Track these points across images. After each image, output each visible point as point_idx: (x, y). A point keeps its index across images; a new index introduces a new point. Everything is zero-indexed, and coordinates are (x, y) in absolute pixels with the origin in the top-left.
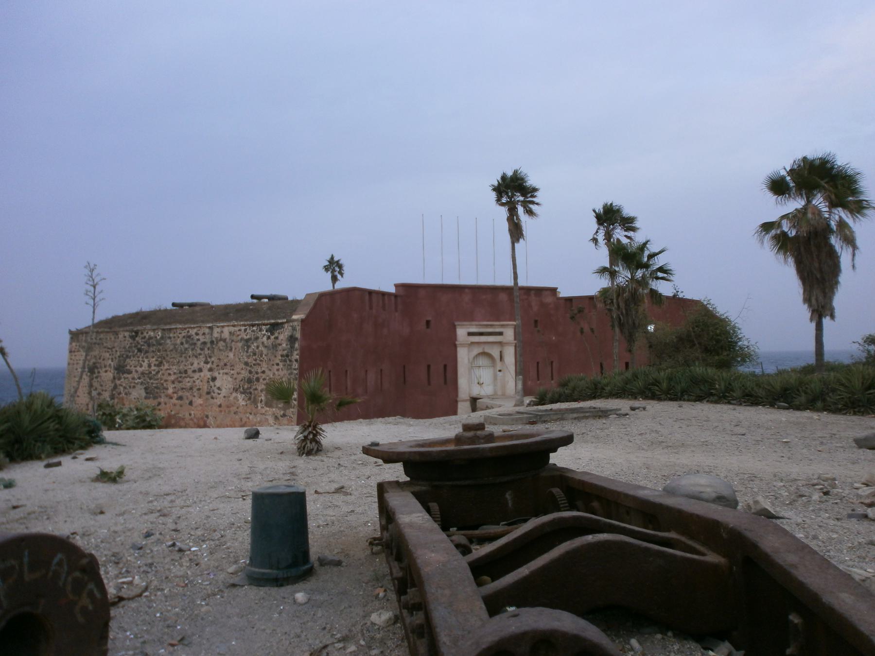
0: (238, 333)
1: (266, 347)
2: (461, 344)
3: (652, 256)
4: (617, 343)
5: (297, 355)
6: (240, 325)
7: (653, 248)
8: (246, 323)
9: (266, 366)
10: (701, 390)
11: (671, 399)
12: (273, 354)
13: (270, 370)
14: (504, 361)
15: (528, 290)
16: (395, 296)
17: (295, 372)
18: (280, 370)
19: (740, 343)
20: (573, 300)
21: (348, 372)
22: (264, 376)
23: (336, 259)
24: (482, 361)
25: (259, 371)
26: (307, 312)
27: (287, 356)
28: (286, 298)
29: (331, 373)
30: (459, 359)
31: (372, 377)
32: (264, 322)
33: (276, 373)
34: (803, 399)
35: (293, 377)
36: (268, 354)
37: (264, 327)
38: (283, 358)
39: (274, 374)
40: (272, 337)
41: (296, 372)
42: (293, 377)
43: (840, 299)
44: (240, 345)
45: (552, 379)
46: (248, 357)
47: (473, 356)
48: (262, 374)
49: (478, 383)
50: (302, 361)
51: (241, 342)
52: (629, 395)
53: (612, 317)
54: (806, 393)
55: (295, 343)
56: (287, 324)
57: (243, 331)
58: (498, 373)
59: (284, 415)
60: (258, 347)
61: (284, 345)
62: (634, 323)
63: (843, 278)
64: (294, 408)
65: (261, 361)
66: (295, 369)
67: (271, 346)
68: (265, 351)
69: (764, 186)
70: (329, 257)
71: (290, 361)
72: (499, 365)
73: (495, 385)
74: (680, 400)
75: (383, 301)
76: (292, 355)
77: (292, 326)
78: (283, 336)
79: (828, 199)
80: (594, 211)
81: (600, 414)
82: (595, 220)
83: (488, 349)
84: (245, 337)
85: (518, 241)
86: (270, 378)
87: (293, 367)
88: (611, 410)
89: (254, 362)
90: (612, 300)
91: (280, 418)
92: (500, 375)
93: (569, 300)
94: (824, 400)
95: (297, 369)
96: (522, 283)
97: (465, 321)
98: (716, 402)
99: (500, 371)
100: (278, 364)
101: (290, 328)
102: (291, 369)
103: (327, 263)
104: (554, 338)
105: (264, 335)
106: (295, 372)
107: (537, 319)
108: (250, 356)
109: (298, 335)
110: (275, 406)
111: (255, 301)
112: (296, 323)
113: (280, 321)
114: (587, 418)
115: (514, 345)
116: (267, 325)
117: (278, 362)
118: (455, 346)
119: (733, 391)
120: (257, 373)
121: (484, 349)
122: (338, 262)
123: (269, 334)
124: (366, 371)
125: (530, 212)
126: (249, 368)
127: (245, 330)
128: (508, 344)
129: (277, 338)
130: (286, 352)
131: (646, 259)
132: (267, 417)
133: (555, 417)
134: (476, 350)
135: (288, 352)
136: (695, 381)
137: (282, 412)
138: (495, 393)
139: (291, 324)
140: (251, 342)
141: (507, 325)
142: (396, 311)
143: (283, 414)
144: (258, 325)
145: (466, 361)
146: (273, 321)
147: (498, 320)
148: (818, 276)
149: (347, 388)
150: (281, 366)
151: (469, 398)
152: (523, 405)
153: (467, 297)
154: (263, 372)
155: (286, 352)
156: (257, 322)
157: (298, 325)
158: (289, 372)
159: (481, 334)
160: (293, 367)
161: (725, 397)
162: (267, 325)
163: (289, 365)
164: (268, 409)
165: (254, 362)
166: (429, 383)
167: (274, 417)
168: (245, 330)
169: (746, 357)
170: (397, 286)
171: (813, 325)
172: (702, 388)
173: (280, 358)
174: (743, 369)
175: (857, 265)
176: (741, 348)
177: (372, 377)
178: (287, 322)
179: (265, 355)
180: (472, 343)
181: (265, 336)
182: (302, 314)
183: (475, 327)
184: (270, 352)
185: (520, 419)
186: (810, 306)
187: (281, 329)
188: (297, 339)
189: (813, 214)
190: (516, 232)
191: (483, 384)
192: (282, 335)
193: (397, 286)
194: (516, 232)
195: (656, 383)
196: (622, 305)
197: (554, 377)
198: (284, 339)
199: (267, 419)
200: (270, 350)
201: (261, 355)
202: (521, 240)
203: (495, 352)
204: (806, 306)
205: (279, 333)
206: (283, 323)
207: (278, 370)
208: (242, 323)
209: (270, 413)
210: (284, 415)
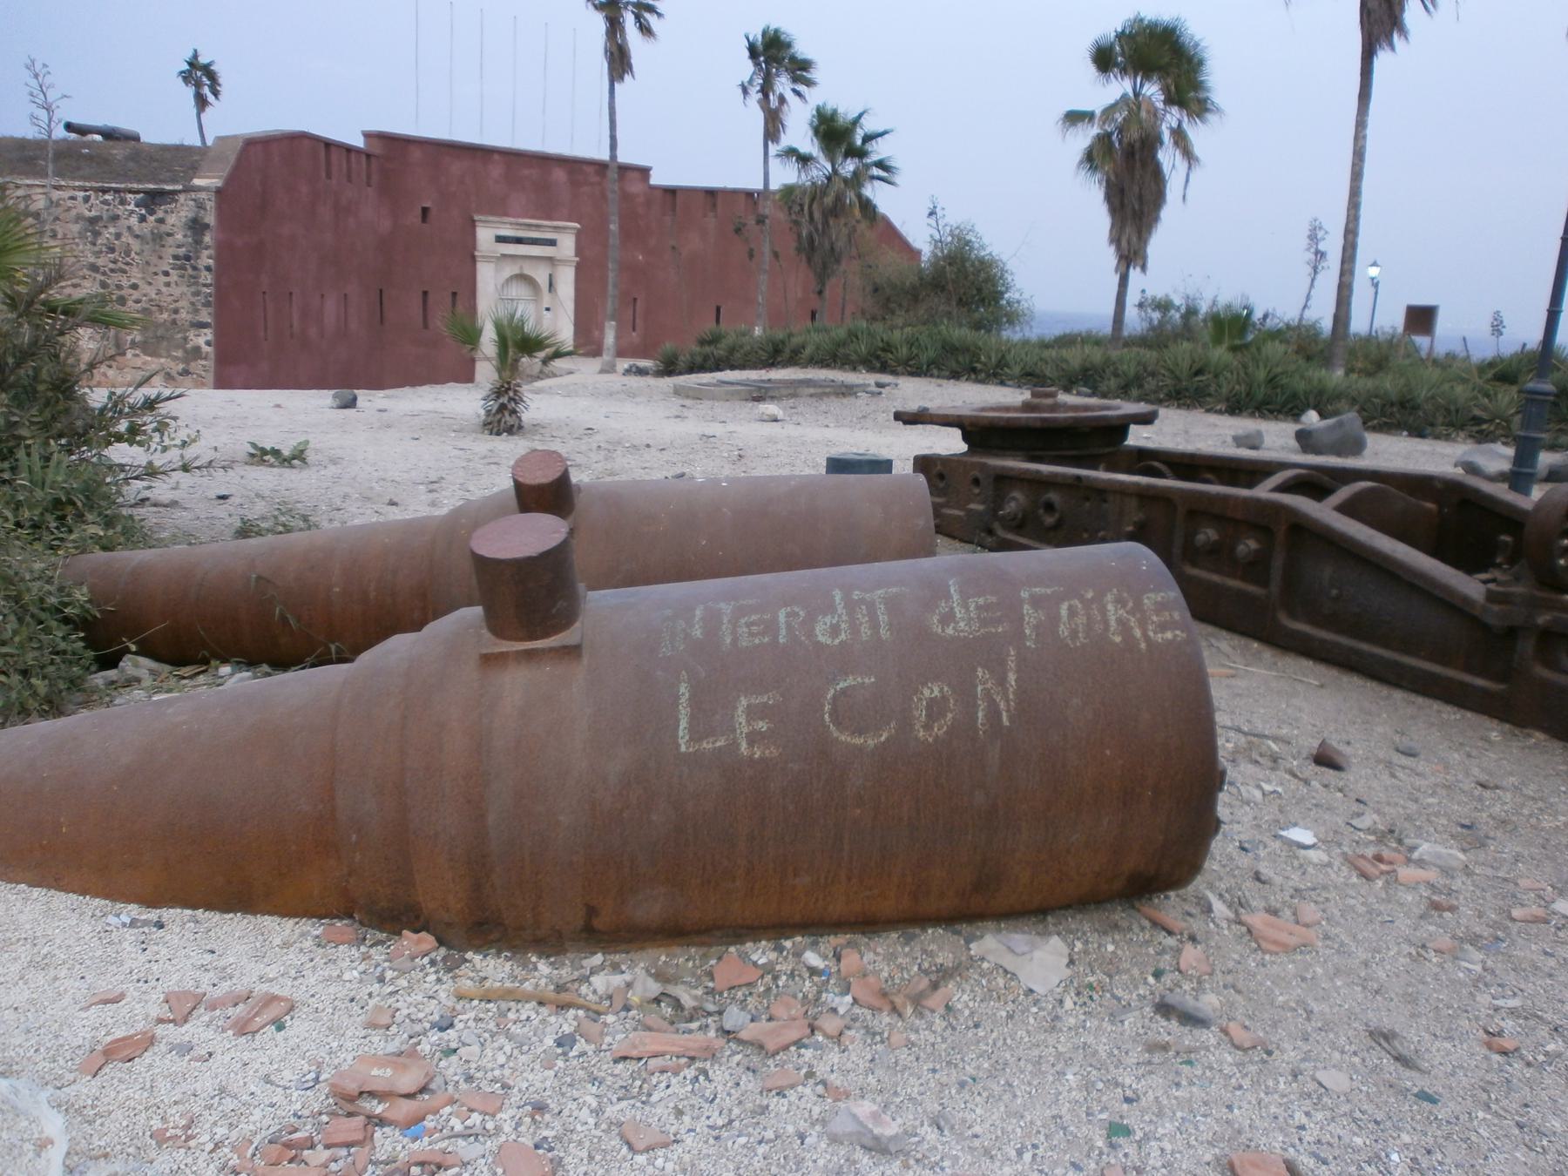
0: (70, 203)
1: (137, 237)
2: (483, 257)
3: (868, 138)
5: (210, 257)
6: (74, 188)
7: (869, 125)
8: (87, 184)
10: (958, 362)
11: (912, 374)
13: (150, 284)
15: (625, 169)
18: (173, 285)
19: (1006, 296)
20: (678, 194)
22: (136, 295)
23: (203, 60)
25: (125, 283)
26: (225, 174)
27: (188, 258)
28: (136, 138)
31: (331, 307)
32: (130, 186)
33: (164, 289)
34: (1113, 383)
37: (129, 196)
39: (159, 292)
40: (152, 218)
43: (1158, 244)
44: (75, 228)
45: (634, 330)
46: (98, 254)
48: (131, 291)
51: (77, 222)
52: (843, 364)
53: (799, 235)
54: (1116, 375)
57: (80, 199)
60: (118, 236)
61: (179, 236)
62: (832, 248)
63: (1166, 213)
64: (206, 359)
65: (127, 264)
66: (205, 285)
67: (149, 236)
68: (136, 245)
69: (1087, 55)
70: (189, 55)
71: (195, 268)
72: (547, 300)
74: (926, 375)
75: (348, 161)
78: (177, 217)
79: (1166, 90)
81: (844, 390)
82: (747, 53)
83: (529, 270)
84: (87, 214)
85: (622, 78)
86: (151, 300)
87: (201, 281)
88: (857, 386)
89: (112, 266)
90: (801, 206)
93: (671, 192)
94: (1141, 386)
96: (624, 157)
97: (493, 214)
98: (982, 382)
99: (548, 309)
100: (166, 274)
102: (196, 284)
103: (186, 67)
105: (132, 212)
108: (101, 252)
109: (210, 218)
110: (164, 353)
111: (73, 136)
112: (203, 195)
114: (827, 395)
116: (137, 192)
117: (167, 268)
118: (473, 259)
119: (1009, 367)
120: (119, 287)
121: (521, 268)
124: (323, 296)
125: (646, 30)
126: (99, 277)
127: (87, 199)
128: (564, 262)
129: (161, 221)
131: (859, 142)
133: (784, 392)
134: (510, 270)
136: (950, 349)
137: (181, 367)
140: (101, 224)
141: (565, 228)
142: (369, 185)
144: (117, 191)
146: (151, 186)
147: (550, 218)
148: (1137, 207)
149: (291, 326)
152: (615, 371)
153: (496, 170)
154: (135, 287)
156: (114, 185)
158: (193, 289)
159: (519, 241)
160: (201, 281)
161: (995, 375)
162: (137, 192)
165: (112, 266)
166: (426, 326)
168: (87, 199)
169: (1013, 317)
171: (1116, 279)
172: (961, 359)
174: (1011, 334)
175: (1187, 197)
176: (1008, 302)
177: (331, 307)
178: (186, 190)
180: (504, 256)
185: (738, 392)
186: (1119, 248)
188: (207, 226)
189: (1148, 112)
190: (619, 62)
194: (619, 62)
195: (888, 347)
196: (817, 215)
197: (637, 328)
198: (178, 224)
201: (128, 253)
202: (627, 77)
203: (540, 275)
204: (1113, 248)
207: (168, 284)
208: (77, 184)
210: (186, 373)
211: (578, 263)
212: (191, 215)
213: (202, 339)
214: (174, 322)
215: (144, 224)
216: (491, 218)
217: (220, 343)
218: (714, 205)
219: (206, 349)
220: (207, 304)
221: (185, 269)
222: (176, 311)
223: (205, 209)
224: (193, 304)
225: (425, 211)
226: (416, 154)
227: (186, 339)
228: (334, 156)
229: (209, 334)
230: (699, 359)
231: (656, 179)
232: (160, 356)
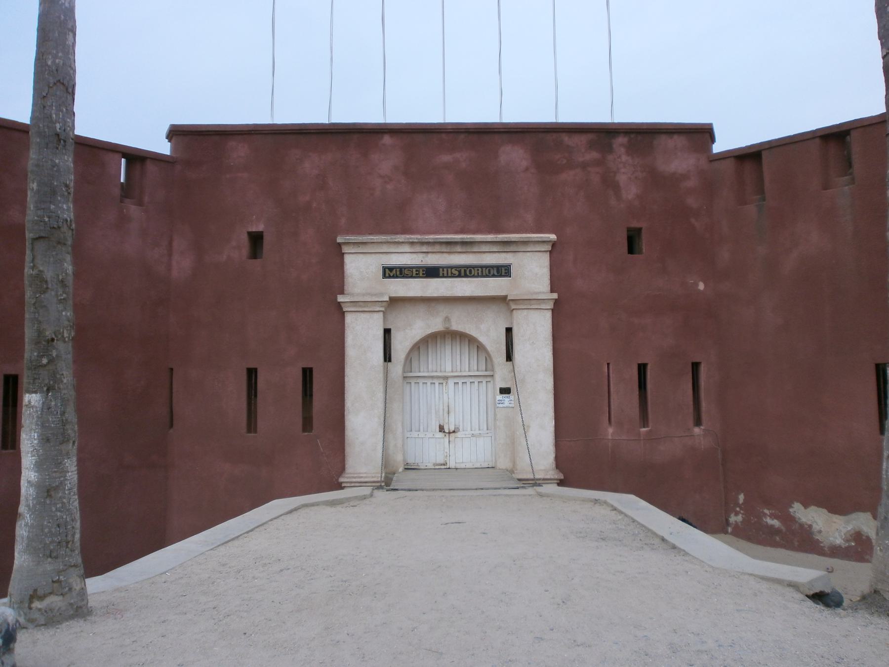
45: (698, 422)
72: (502, 375)
83: (461, 321)
92: (507, 403)
99: (505, 391)
107: (635, 224)
115: (550, 305)
118: (340, 312)
121: (447, 319)
128: (528, 302)
141: (525, 243)
159: (432, 272)
183: (407, 248)
193: (176, 133)
197: (704, 417)
211: (556, 302)
225: (256, 239)
226: (239, 151)
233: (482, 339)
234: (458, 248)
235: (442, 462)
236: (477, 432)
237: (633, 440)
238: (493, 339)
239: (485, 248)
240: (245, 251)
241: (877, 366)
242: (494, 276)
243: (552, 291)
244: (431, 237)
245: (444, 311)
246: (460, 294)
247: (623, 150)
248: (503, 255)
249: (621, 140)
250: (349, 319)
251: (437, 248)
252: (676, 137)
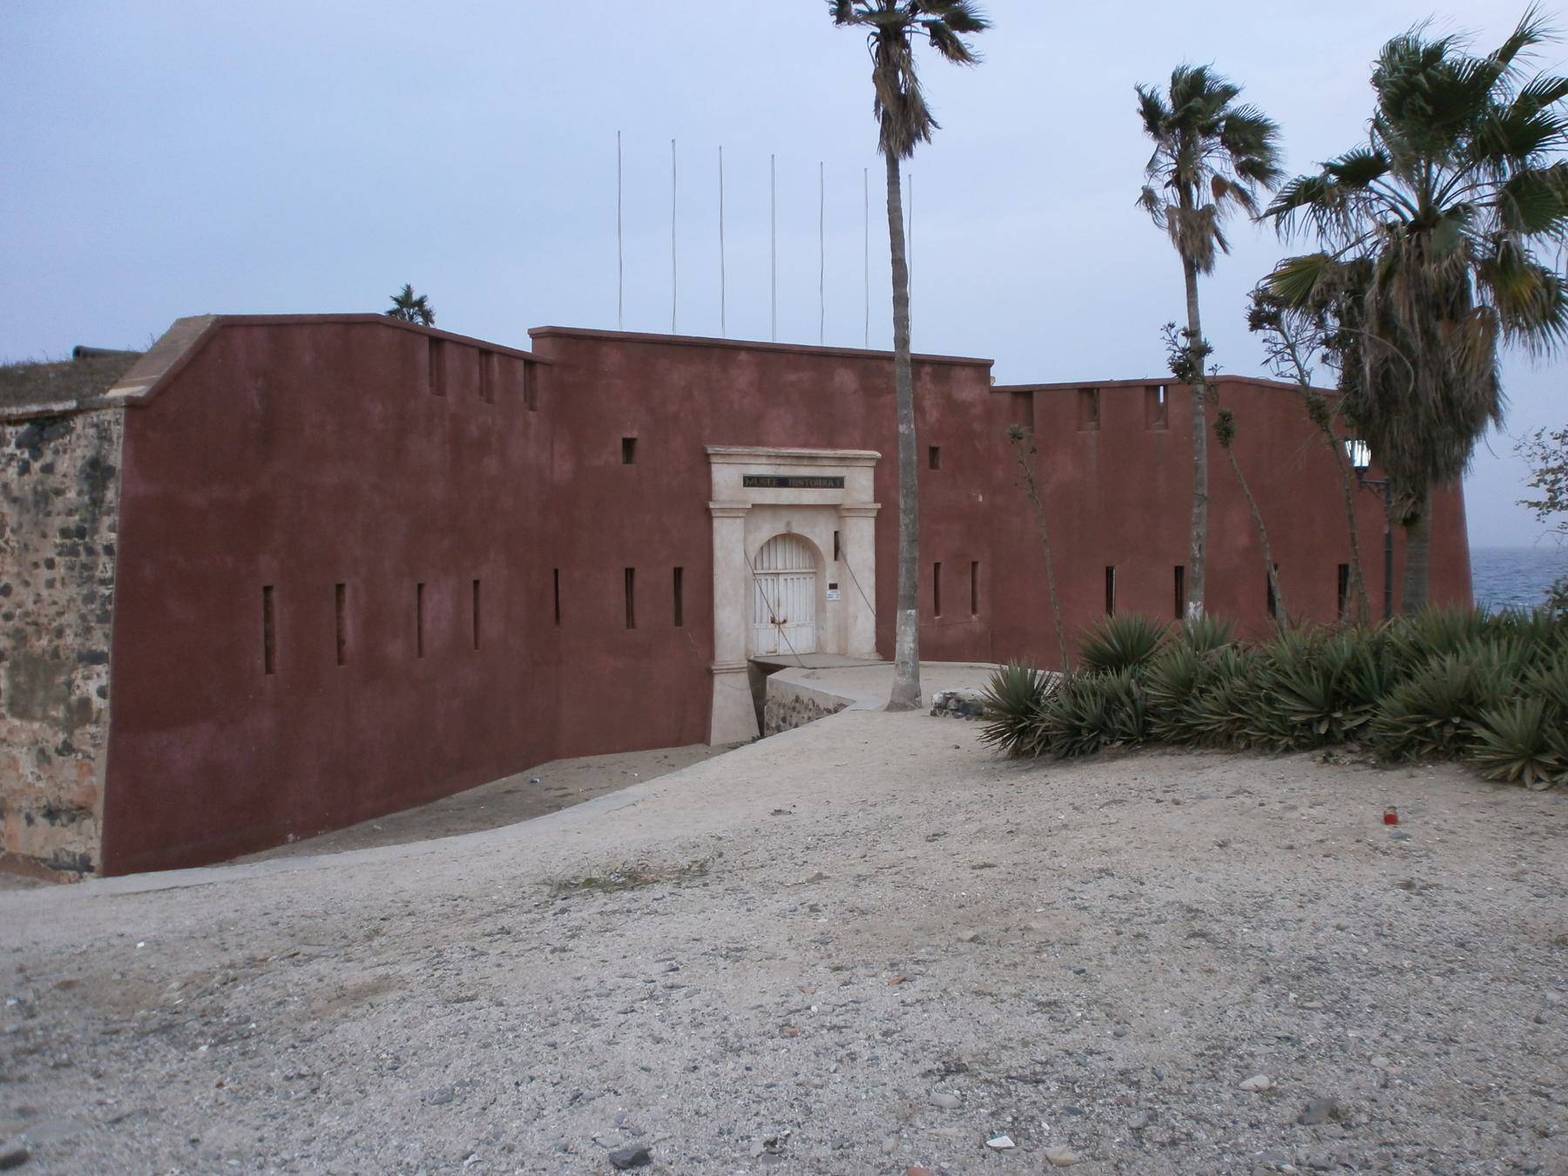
1: (15, 500)
4: (1204, 509)
9: (15, 570)
12: (36, 524)
13: (27, 584)
14: (846, 561)
16: (529, 362)
17: (105, 591)
18: (58, 585)
20: (1035, 395)
21: (348, 592)
24: (784, 559)
27: (81, 533)
29: (275, 595)
30: (719, 554)
31: (440, 606)
35: (98, 612)
36: (21, 526)
38: (68, 542)
40: (36, 466)
41: (107, 593)
42: (98, 612)
45: (974, 611)
47: (757, 545)
49: (773, 621)
50: (130, 553)
55: (105, 487)
56: (80, 417)
58: (829, 592)
59: (67, 749)
64: (97, 722)
66: (103, 582)
67: (30, 497)
71: (91, 551)
72: (831, 572)
73: (819, 627)
76: (95, 531)
77: (96, 426)
80: (1139, 90)
82: (1141, 122)
83: (801, 526)
85: (908, 149)
86: (27, 614)
87: (98, 574)
91: (54, 756)
92: (834, 597)
93: (1024, 395)
95: (110, 581)
97: (740, 444)
99: (833, 586)
100: (50, 564)
101: (92, 431)
102: (90, 579)
104: (981, 499)
105: (12, 457)
106: (105, 591)
107: (935, 444)
109: (116, 458)
110: (38, 712)
112: (108, 415)
113: (57, 407)
115: (874, 514)
116: (18, 422)
118: (708, 515)
121: (788, 524)
122: (420, 303)
123: (26, 455)
124: (420, 586)
128: (856, 511)
129: (48, 469)
130: (77, 518)
132: (15, 752)
134: (768, 528)
135: (83, 520)
137: (61, 737)
138: (819, 650)
139: (95, 420)
141: (856, 459)
143: (65, 742)
145: (739, 557)
146: (35, 408)
147: (831, 445)
150: (60, 571)
151: (745, 663)
153: (743, 376)
155: (77, 518)
157: (117, 422)
159: (783, 482)
160: (98, 574)
162: (18, 422)
163: (84, 567)
164: (17, 722)
166: (631, 622)
167: (34, 751)
170: (536, 335)
173: (58, 541)
177: (440, 606)
179: (13, 531)
180: (757, 507)
181: (14, 463)
182: (141, 383)
183: (764, 460)
184: (27, 518)
187: (62, 436)
188: (110, 471)
191: (785, 621)
192: (67, 456)
193: (536, 335)
197: (979, 606)
198: (72, 471)
199: (14, 759)
200: (28, 511)
203: (821, 535)
205: (56, 452)
206: (66, 416)
207: (50, 584)
209: (23, 736)
210: (67, 749)
211: (879, 511)
212: (90, 453)
213: (93, 684)
214: (56, 653)
215: (26, 477)
216: (734, 450)
217: (119, 691)
218: (1095, 411)
219: (99, 703)
220: (103, 619)
221: (77, 554)
222: (60, 633)
223: (110, 440)
224: (83, 618)
225: (629, 444)
226: (612, 358)
227: (69, 684)
228: (452, 360)
229: (101, 676)
230: (1093, 708)
231: (1002, 377)
232: (32, 718)
233: (817, 541)
234: (805, 462)
235: (772, 649)
236: (801, 623)
237: (476, 600)
238: (824, 541)
239: (825, 462)
240: (620, 458)
241: (1107, 568)
242: (831, 487)
243: (876, 501)
244: (784, 451)
245: (786, 516)
246: (805, 502)
247: (928, 378)
248: (839, 469)
249: (927, 369)
250: (717, 523)
251: (789, 461)
252: (967, 369)
